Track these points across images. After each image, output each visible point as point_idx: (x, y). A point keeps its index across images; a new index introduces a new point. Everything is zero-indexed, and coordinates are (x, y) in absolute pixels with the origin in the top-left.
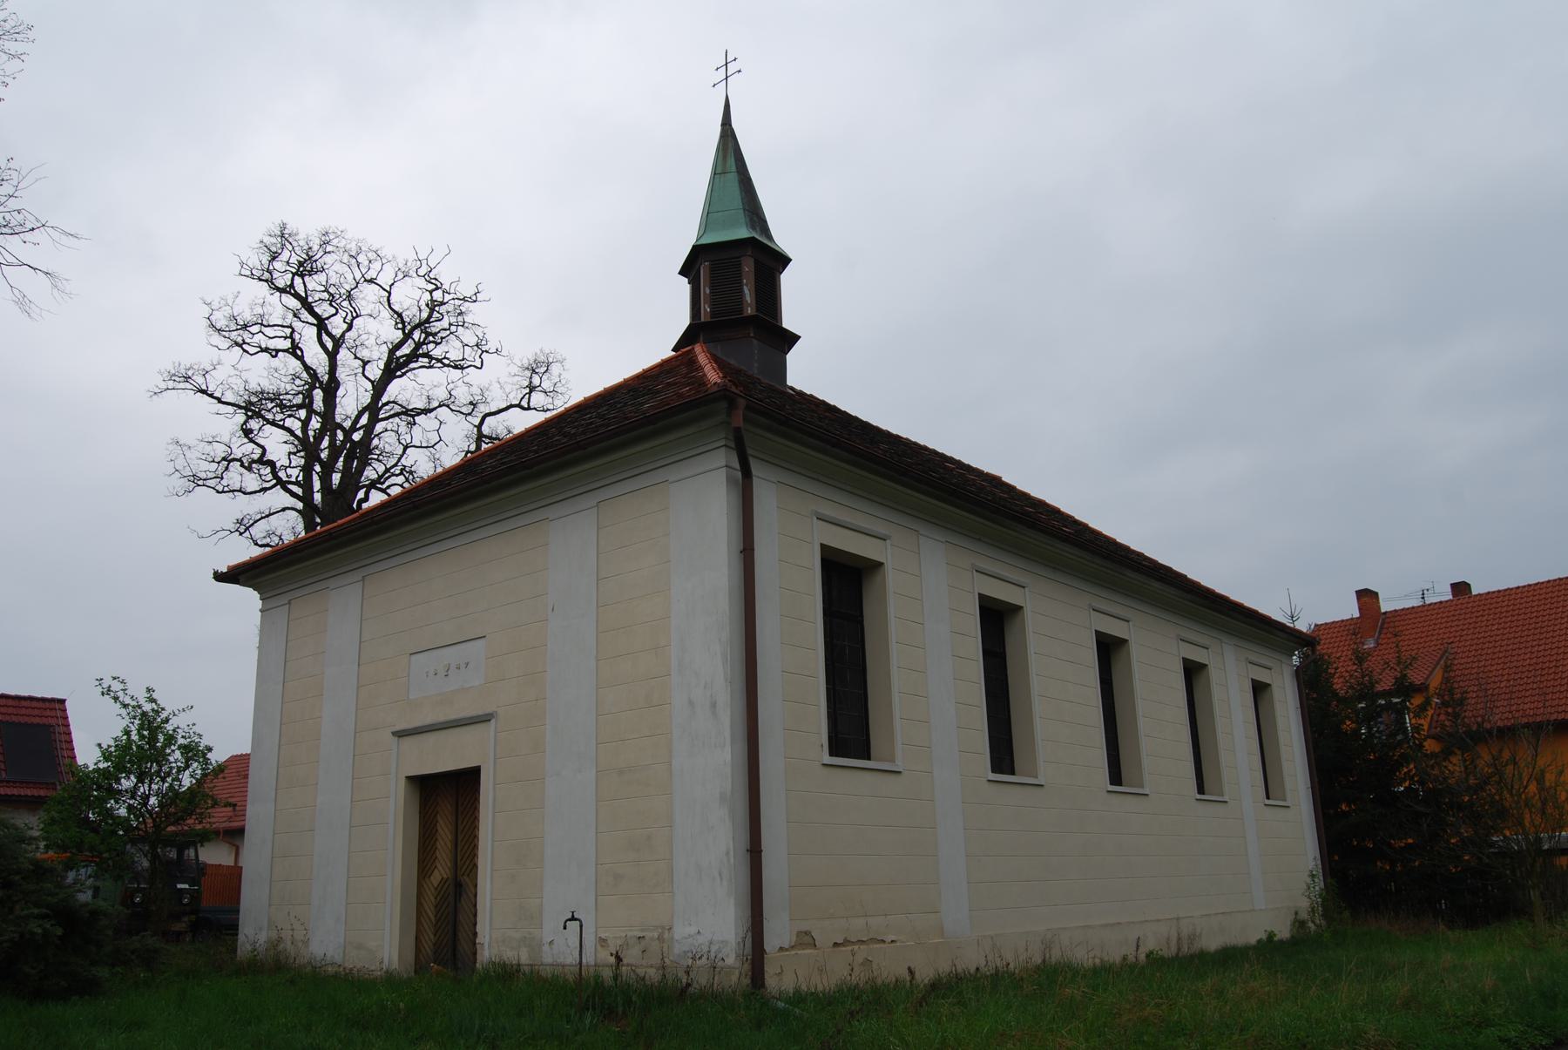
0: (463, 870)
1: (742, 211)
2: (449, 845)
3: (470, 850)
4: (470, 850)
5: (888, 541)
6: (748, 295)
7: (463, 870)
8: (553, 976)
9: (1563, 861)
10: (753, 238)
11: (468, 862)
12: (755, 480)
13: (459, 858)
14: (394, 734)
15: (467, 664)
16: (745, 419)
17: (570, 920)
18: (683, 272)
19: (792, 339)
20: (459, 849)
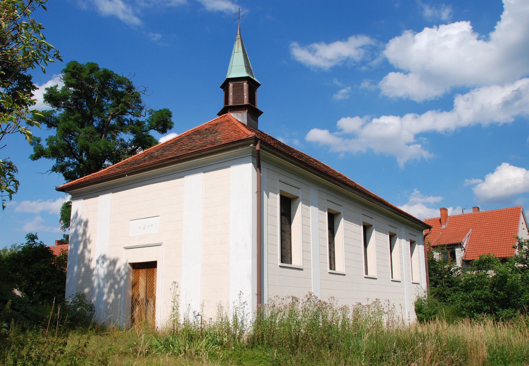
0: (149, 296)
1: (244, 66)
2: (144, 287)
3: (151, 290)
4: (151, 290)
5: (300, 190)
6: (246, 97)
7: (149, 296)
8: (313, 325)
9: (10, 360)
10: (249, 77)
11: (151, 293)
12: (261, 167)
13: (147, 292)
14: (124, 248)
15: (152, 225)
16: (261, 147)
17: (198, 315)
18: (222, 87)
19: (260, 113)
20: (148, 289)
